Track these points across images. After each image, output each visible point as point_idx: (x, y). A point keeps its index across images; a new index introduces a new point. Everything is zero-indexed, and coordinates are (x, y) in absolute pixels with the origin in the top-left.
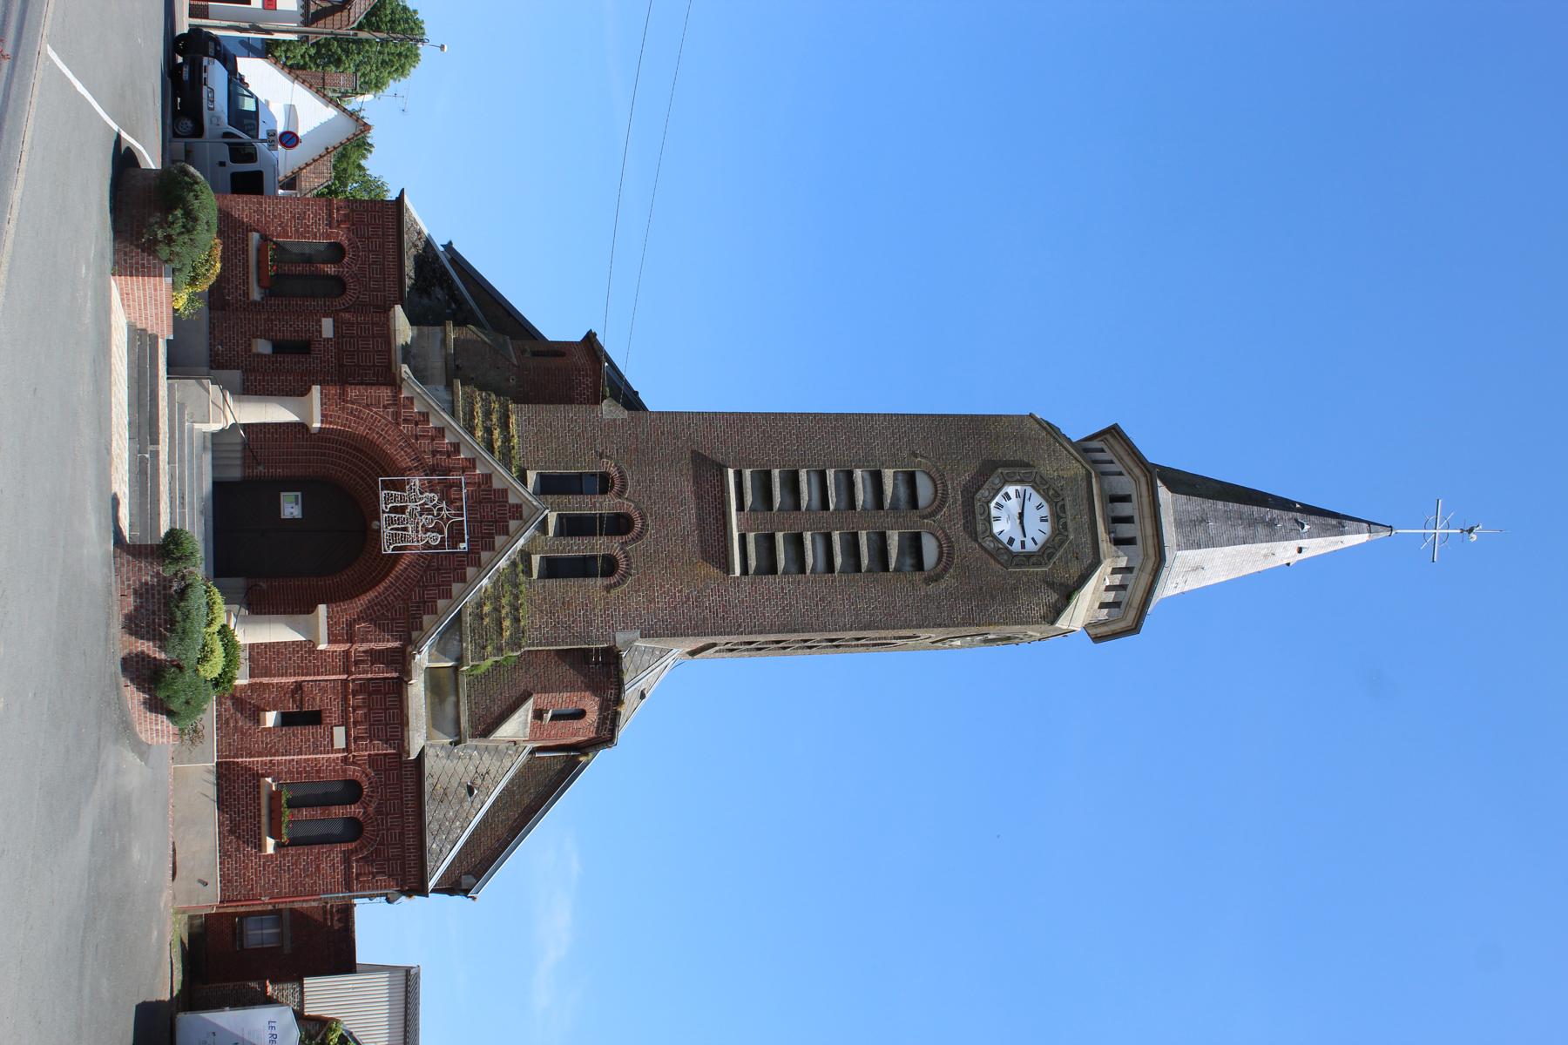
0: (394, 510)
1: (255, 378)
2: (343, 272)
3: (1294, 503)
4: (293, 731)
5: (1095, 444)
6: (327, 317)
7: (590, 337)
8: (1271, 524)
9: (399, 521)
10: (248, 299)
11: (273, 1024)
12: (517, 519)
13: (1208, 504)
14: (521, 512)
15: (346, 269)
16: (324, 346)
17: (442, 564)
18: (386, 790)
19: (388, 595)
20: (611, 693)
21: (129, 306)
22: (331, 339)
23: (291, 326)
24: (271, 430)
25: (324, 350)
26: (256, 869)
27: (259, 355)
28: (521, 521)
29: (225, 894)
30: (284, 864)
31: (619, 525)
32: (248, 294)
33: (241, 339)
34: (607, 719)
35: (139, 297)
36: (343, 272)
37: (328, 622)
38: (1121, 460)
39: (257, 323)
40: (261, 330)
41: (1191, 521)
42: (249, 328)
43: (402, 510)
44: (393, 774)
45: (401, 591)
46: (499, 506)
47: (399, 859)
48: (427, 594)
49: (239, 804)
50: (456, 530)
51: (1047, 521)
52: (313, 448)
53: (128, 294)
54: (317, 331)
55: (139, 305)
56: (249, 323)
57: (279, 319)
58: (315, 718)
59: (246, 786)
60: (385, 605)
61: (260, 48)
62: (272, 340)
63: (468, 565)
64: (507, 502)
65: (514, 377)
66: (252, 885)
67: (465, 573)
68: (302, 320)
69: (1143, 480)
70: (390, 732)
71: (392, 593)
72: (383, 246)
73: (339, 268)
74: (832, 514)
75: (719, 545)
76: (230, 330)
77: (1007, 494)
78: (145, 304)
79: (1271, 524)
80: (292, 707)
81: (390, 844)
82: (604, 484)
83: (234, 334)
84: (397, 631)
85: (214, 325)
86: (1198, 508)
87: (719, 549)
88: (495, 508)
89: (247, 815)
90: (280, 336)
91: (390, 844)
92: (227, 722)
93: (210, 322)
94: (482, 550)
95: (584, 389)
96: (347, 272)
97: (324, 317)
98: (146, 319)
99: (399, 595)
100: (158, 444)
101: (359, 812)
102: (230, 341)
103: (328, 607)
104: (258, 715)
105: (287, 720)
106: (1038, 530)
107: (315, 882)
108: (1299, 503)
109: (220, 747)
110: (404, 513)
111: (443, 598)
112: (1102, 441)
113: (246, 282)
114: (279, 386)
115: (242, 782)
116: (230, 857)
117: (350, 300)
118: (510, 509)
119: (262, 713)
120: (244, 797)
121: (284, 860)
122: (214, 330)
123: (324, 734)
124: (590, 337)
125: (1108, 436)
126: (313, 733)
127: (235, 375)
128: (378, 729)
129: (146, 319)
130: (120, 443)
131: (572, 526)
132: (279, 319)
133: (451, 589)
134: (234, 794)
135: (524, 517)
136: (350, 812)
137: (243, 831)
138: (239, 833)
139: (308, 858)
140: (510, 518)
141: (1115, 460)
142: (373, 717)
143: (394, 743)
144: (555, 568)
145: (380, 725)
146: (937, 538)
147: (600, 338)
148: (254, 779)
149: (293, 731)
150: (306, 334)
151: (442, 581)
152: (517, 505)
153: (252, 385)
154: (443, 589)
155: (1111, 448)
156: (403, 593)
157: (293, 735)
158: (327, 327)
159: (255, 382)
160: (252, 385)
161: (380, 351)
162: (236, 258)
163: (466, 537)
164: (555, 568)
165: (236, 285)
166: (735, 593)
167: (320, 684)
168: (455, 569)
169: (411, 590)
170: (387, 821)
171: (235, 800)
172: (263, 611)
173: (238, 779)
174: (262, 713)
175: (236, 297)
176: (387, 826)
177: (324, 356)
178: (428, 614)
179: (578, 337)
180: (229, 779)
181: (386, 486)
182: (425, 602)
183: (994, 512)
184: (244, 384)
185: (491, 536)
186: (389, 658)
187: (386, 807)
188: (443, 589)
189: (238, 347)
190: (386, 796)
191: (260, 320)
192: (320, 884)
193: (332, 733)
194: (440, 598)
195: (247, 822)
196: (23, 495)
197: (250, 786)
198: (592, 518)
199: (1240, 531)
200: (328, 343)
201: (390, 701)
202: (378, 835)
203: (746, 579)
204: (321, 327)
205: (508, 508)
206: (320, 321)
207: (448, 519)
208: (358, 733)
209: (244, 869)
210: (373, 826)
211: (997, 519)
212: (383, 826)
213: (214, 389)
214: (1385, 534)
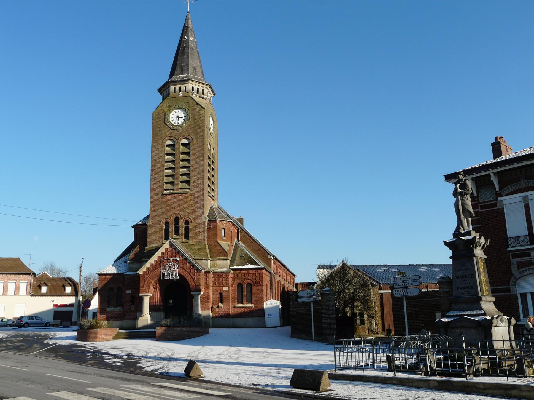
0: (169, 276)
3: (180, 41)
8: (184, 48)
9: (172, 275)
13: (178, 66)
24: (399, 328)
31: (177, 220)
38: (166, 90)
43: (169, 274)
58: (221, 294)
61: (487, 369)
74: (176, 166)
77: (172, 121)
79: (184, 48)
82: (167, 224)
86: (179, 68)
105: (221, 301)
106: (181, 114)
110: (170, 273)
127: (138, 314)
131: (177, 232)
141: (166, 91)
144: (187, 236)
158: (129, 292)
163: (176, 258)
164: (187, 236)
172: (395, 324)
179: (133, 230)
181: (163, 277)
196: (232, 380)
198: (175, 227)
199: (185, 57)
203: (191, 189)
207: (172, 263)
213: (140, 318)
214: (189, 15)
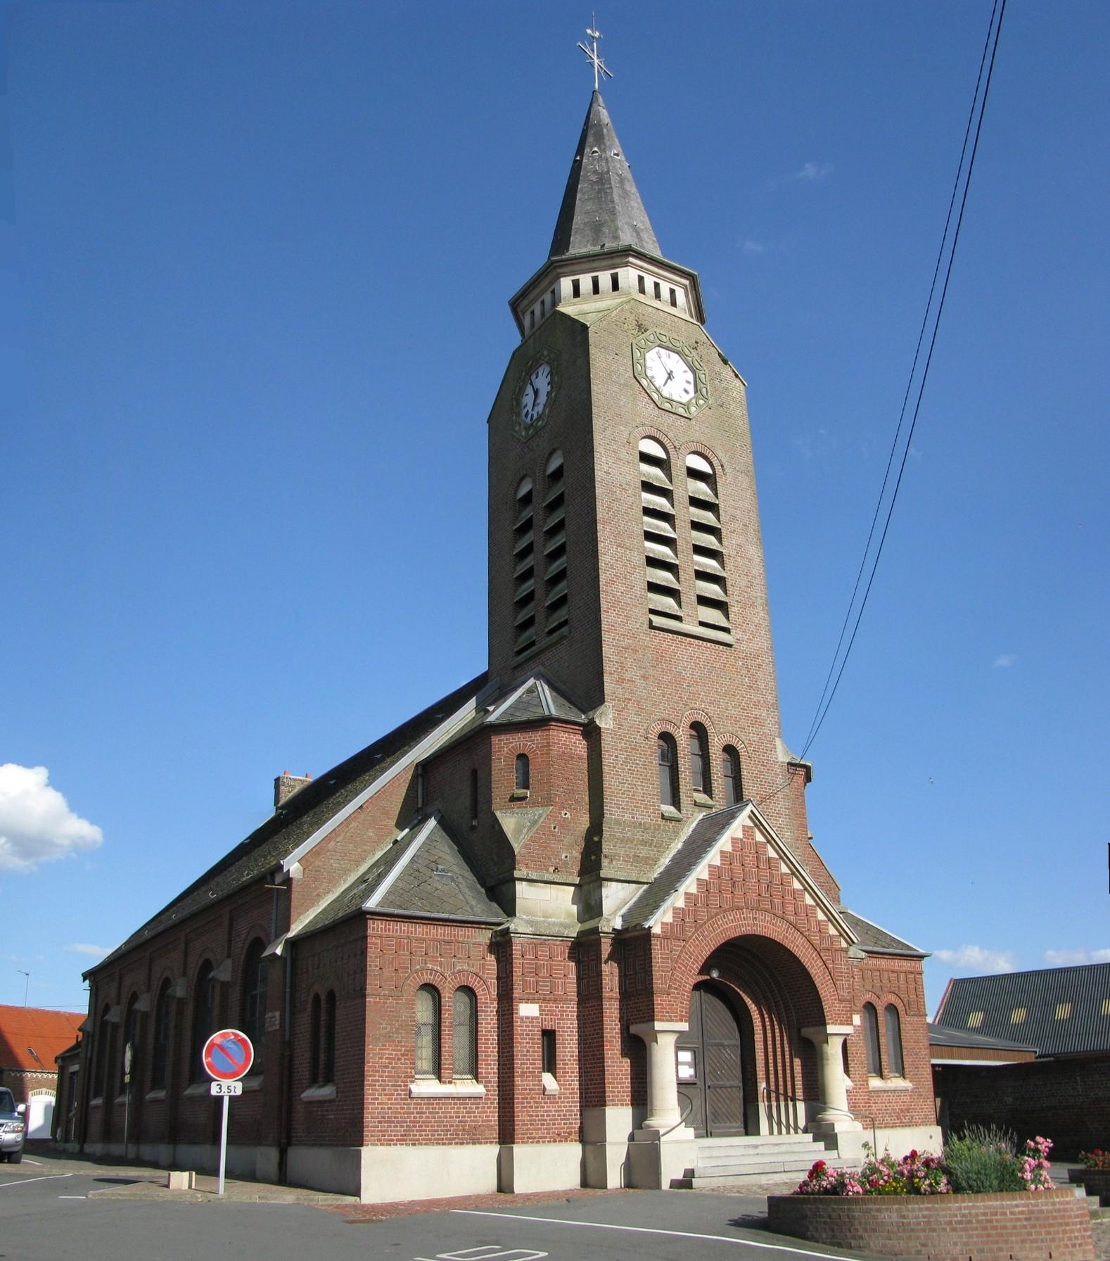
3: (575, 161)
5: (527, 322)
7: (86, 976)
16: (546, 1015)
22: (540, 1006)
23: (528, 1051)
65: (563, 813)
71: (815, 962)
74: (679, 537)
93: (527, 1142)
103: (829, 1024)
112: (523, 315)
117: (478, 983)
118: (746, 838)
122: (535, 1138)
124: (86, 976)
130: (340, 1068)
132: (521, 1064)
141: (541, 299)
165: (467, 1112)
177: (556, 1015)
189: (551, 1111)
204: (527, 1018)
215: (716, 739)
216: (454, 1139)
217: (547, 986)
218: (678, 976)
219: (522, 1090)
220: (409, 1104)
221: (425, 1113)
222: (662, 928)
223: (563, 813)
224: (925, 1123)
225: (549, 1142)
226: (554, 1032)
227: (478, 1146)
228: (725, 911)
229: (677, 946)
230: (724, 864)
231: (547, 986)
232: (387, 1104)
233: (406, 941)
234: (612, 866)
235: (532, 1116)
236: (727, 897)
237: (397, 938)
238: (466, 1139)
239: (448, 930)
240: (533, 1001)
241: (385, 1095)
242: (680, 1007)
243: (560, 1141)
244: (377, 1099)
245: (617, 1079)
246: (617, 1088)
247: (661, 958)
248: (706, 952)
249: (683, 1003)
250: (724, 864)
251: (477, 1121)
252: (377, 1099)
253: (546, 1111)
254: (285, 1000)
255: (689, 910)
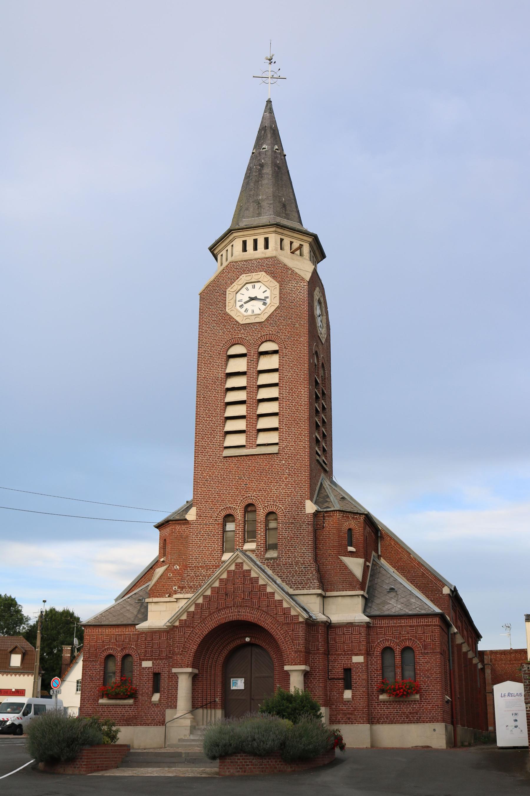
1: (170, 702)
2: (120, 656)
4: (354, 683)
6: (141, 664)
10: (132, 705)
11: (503, 695)
12: (243, 565)
14: (239, 563)
15: (119, 654)
17: (265, 605)
18: (388, 635)
19: (280, 633)
20: (339, 515)
21: (106, 767)
22: (153, 662)
23: (146, 683)
25: (159, 666)
26: (427, 703)
27: (160, 700)
28: (244, 563)
29: (440, 720)
30: (425, 688)
32: (130, 705)
33: (152, 709)
34: (354, 517)
35: (101, 761)
36: (120, 656)
37: (293, 665)
38: (226, 246)
39: (144, 701)
40: (148, 699)
41: (258, 208)
42: (146, 705)
44: (379, 631)
45: (278, 627)
46: (236, 575)
47: (424, 628)
48: (280, 613)
49: (393, 713)
50: (247, 597)
51: (254, 286)
52: (207, 672)
53: (98, 767)
54: (148, 670)
55: (106, 761)
56: (144, 705)
57: (142, 689)
59: (384, 708)
60: (285, 635)
62: (344, 690)
63: (266, 591)
64: (234, 571)
65: (175, 566)
66: (436, 705)
67: (270, 593)
68: (143, 678)
69: (235, 235)
70: (356, 632)
71: (275, 630)
72: (107, 634)
73: (118, 658)
75: (262, 459)
76: (147, 715)
78: (106, 758)
80: (341, 684)
81: (416, 632)
83: (149, 713)
84: (299, 629)
85: (144, 723)
87: (265, 459)
88: (237, 577)
89: (398, 708)
90: (151, 689)
91: (416, 632)
92: (349, 718)
93: (143, 725)
94: (258, 584)
95: (182, 530)
96: (120, 653)
97: (141, 666)
98: (116, 758)
99: (280, 628)
100: (181, 753)
101: (399, 649)
102: (153, 715)
103: (286, 665)
104: (345, 702)
107: (435, 672)
108: (253, 150)
109: (362, 722)
111: (282, 604)
113: (124, 706)
114: (174, 690)
115: (382, 711)
116: (420, 718)
118: (237, 569)
119: (344, 700)
120: (389, 709)
121: (423, 688)
122: (147, 723)
123: (356, 667)
125: (215, 252)
126: (355, 673)
128: (354, 639)
129: (116, 758)
132: (142, 689)
133: (278, 600)
134: (387, 715)
135: (242, 561)
136: (399, 653)
137: (407, 710)
138: (408, 712)
139: (422, 676)
140: (242, 569)
141: (226, 249)
142: (348, 641)
143: (362, 630)
145: (352, 638)
146: (262, 343)
147: (155, 524)
148: (380, 704)
149: (354, 683)
150: (150, 675)
151: (274, 605)
152: (236, 565)
153: (173, 704)
154: (278, 604)
155: (221, 251)
156: (279, 625)
157: (357, 683)
158: (147, 664)
159: (172, 702)
160: (173, 704)
161: (160, 637)
162: (112, 712)
165: (125, 712)
166: (288, 450)
167: (330, 669)
168: (268, 598)
169: (278, 621)
170: (404, 634)
171: (391, 715)
173: (380, 713)
174: (344, 700)
175: (131, 712)
176: (406, 634)
178: (290, 612)
180: (380, 717)
182: (284, 614)
183: (249, 312)
184: (173, 708)
185: (251, 579)
186: (315, 633)
187: (397, 634)
188: (278, 604)
189: (156, 711)
190: (391, 635)
191: (142, 699)
192: (436, 670)
193: (356, 663)
194: (282, 606)
195: (403, 708)
197: (384, 706)
200: (155, 664)
201: (340, 633)
202: (411, 639)
204: (146, 668)
205: (237, 570)
206: (143, 668)
208: (356, 649)
209: (427, 710)
210: (406, 641)
211: (253, 311)
212: (406, 636)
215: (262, 511)
216: (119, 723)
217: (157, 652)
218: (187, 645)
219: (142, 701)
220: (99, 708)
221: (106, 712)
222: (179, 622)
223: (175, 566)
224: (432, 720)
225: (154, 725)
226: (160, 674)
227: (130, 727)
228: (219, 610)
229: (189, 631)
230: (221, 585)
231: (157, 652)
232: (89, 708)
233: (101, 636)
234: (182, 592)
235: (146, 713)
236: (221, 603)
237: (97, 635)
238: (125, 723)
239: (120, 629)
240: (149, 660)
241: (89, 704)
242: (188, 660)
243: (160, 725)
244: (85, 706)
245: (173, 696)
246: (174, 700)
247: (178, 637)
248: (206, 632)
249: (189, 659)
250: (221, 585)
251: (130, 715)
252: (85, 706)
253: (153, 711)
254: (451, 642)
255: (197, 612)
